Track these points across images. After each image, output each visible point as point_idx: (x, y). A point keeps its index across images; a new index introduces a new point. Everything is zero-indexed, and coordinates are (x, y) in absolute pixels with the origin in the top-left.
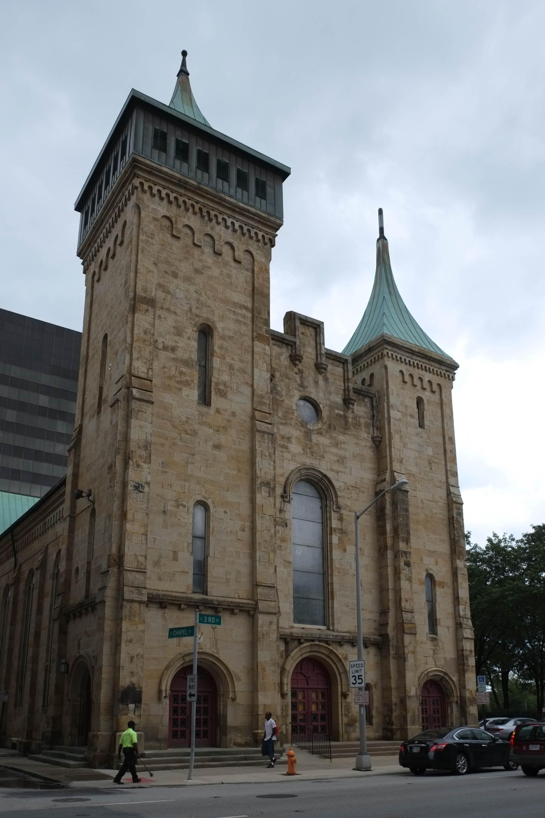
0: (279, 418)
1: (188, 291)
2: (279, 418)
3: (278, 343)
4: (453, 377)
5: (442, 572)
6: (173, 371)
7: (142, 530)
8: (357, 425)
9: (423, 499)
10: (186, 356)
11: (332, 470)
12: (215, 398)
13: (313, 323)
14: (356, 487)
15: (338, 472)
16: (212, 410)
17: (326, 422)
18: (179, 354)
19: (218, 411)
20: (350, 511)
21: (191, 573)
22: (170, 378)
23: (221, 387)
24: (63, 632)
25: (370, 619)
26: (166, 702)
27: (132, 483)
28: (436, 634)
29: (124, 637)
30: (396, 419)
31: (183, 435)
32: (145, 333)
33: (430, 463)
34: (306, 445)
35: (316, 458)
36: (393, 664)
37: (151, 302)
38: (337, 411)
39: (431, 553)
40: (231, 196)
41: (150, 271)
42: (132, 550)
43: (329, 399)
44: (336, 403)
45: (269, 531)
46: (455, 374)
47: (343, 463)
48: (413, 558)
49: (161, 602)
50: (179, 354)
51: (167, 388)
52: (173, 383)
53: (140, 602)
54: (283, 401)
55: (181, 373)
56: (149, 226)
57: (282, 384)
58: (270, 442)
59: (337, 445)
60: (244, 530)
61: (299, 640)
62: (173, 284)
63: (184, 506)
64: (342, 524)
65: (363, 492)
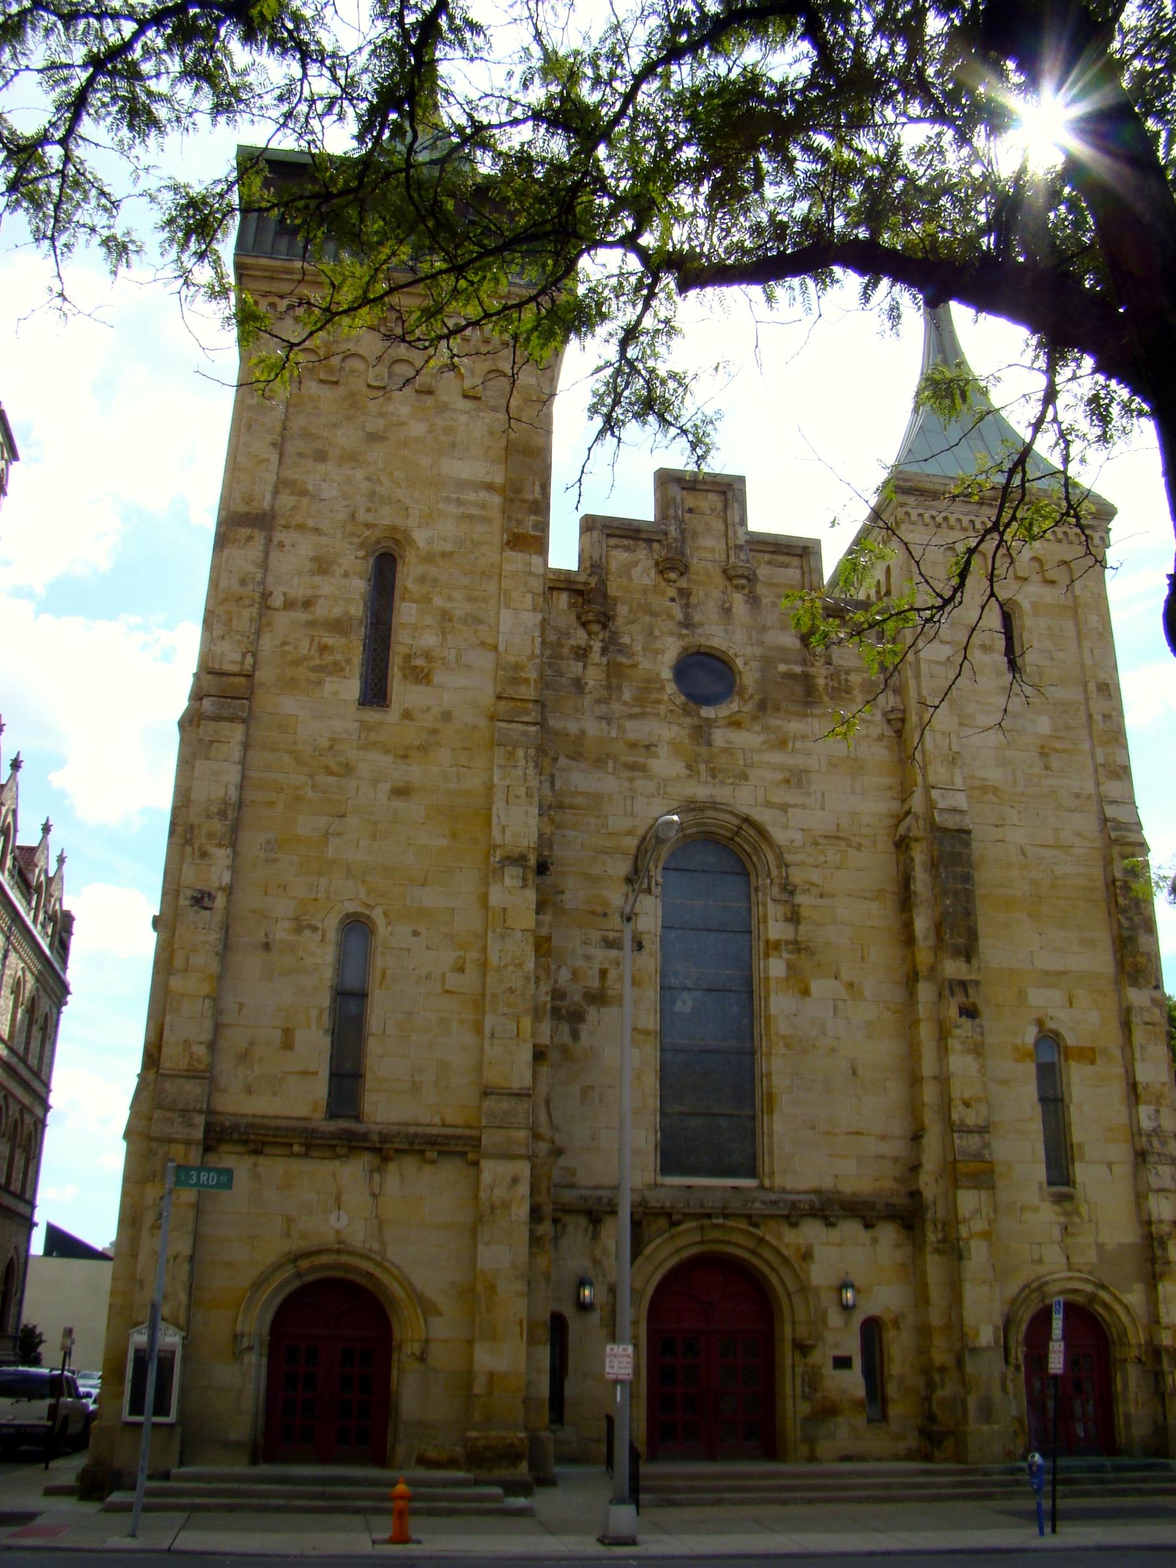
0: (625, 704)
1: (349, 480)
2: (625, 704)
3: (625, 542)
4: (1102, 539)
6: (304, 648)
7: (206, 989)
9: (1020, 847)
10: (337, 612)
11: (768, 804)
12: (400, 691)
13: (714, 483)
14: (837, 838)
15: (784, 808)
16: (392, 715)
17: (751, 697)
19: (407, 715)
20: (821, 896)
22: (297, 663)
23: (419, 662)
25: (882, 1157)
27: (189, 893)
28: (1068, 1181)
30: (937, 663)
31: (324, 779)
33: (1043, 755)
34: (698, 755)
35: (722, 783)
36: (934, 1268)
38: (782, 668)
39: (1050, 978)
41: (262, 461)
43: (761, 643)
44: (781, 649)
45: (520, 965)
46: (1108, 531)
47: (799, 785)
50: (320, 611)
51: (290, 684)
52: (302, 672)
54: (635, 666)
55: (323, 649)
57: (636, 628)
58: (531, 765)
60: (461, 970)
61: (672, 1218)
62: (313, 476)
63: (315, 929)
64: (796, 930)
65: (859, 847)
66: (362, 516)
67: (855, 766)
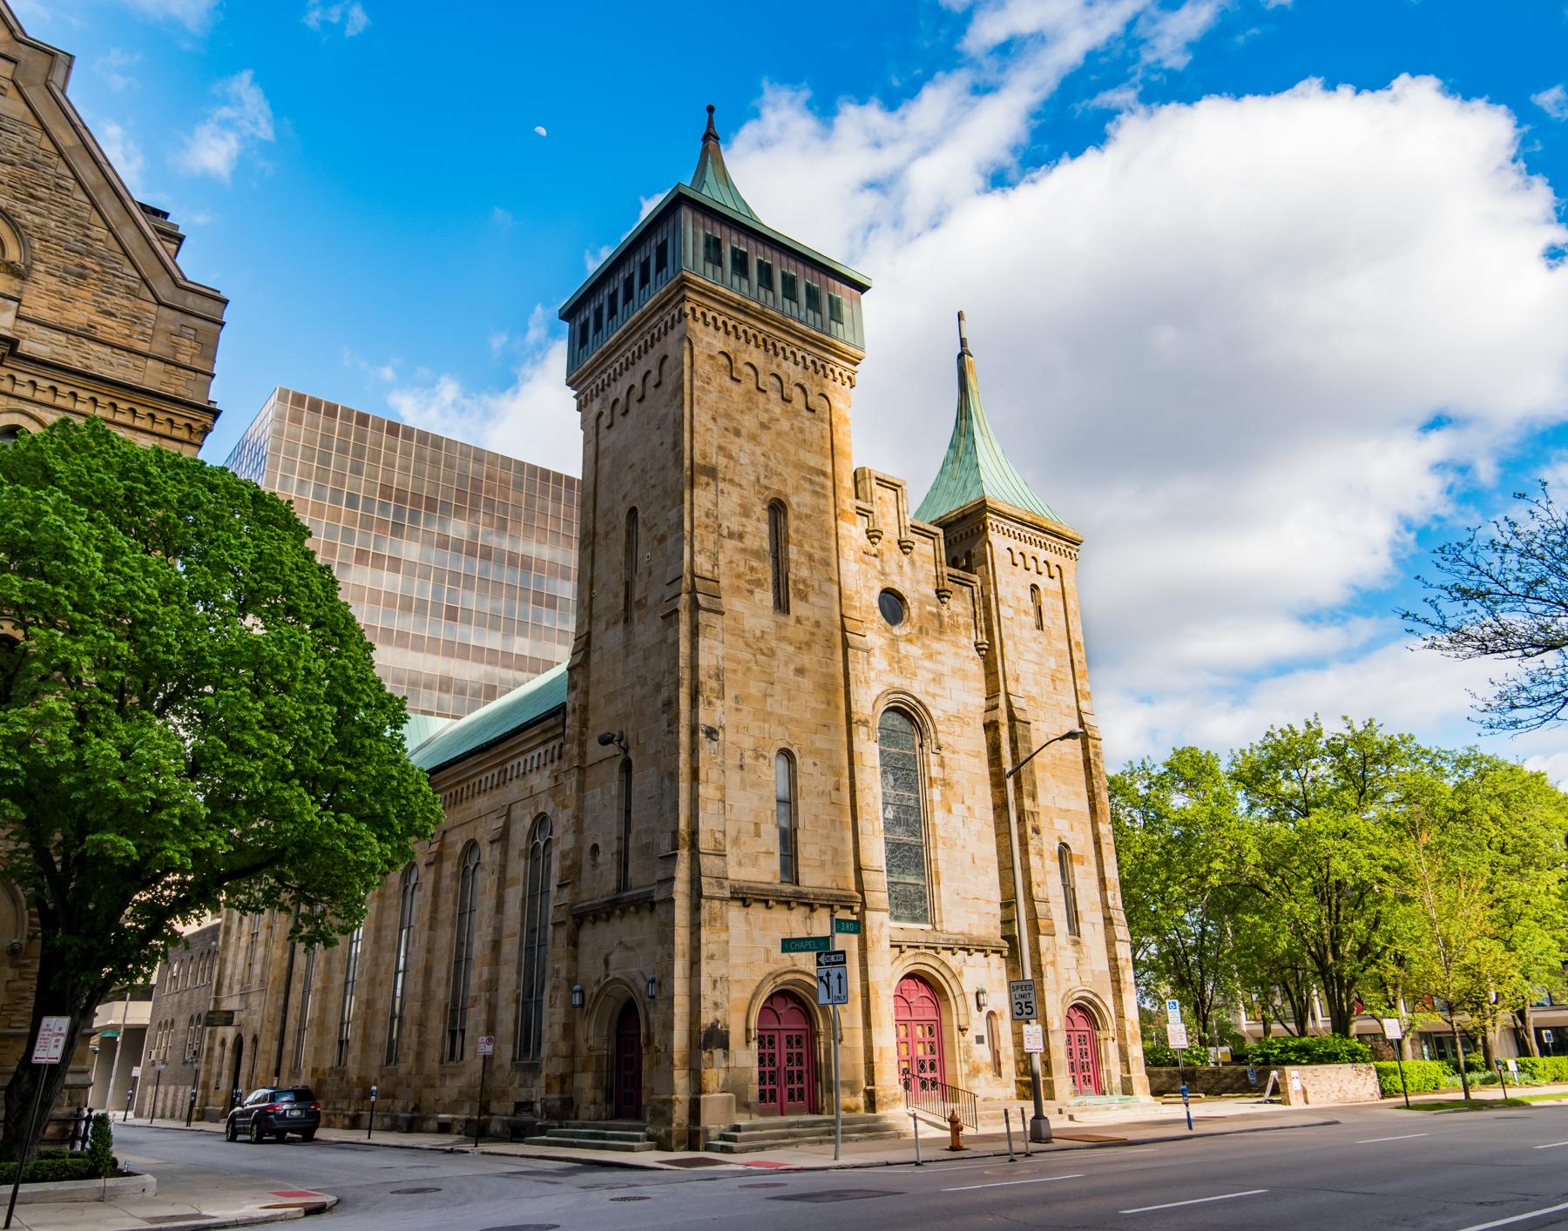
1: (753, 454)
5: (1081, 843)
7: (719, 796)
8: (955, 627)
10: (756, 546)
11: (927, 693)
12: (795, 605)
15: (934, 696)
16: (791, 620)
18: (750, 542)
21: (777, 854)
22: (739, 576)
23: (801, 586)
24: (574, 942)
26: (754, 1045)
29: (704, 952)
31: (760, 657)
32: (707, 515)
37: (712, 472)
38: (928, 608)
39: (1064, 812)
40: (801, 322)
42: (708, 823)
44: (927, 596)
48: (1042, 822)
49: (744, 897)
51: (737, 590)
53: (721, 899)
55: (752, 569)
56: (703, 367)
59: (930, 657)
62: (737, 446)
66: (763, 481)
67: (961, 673)
